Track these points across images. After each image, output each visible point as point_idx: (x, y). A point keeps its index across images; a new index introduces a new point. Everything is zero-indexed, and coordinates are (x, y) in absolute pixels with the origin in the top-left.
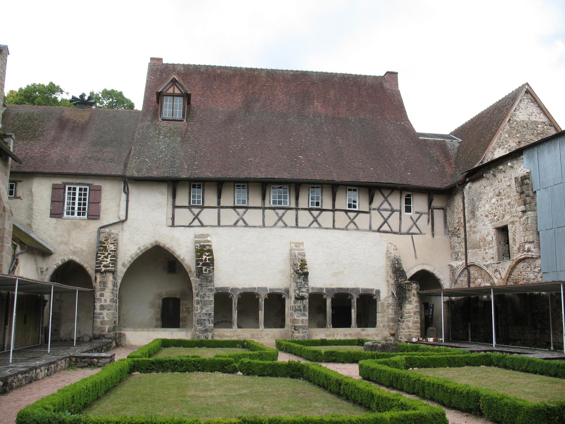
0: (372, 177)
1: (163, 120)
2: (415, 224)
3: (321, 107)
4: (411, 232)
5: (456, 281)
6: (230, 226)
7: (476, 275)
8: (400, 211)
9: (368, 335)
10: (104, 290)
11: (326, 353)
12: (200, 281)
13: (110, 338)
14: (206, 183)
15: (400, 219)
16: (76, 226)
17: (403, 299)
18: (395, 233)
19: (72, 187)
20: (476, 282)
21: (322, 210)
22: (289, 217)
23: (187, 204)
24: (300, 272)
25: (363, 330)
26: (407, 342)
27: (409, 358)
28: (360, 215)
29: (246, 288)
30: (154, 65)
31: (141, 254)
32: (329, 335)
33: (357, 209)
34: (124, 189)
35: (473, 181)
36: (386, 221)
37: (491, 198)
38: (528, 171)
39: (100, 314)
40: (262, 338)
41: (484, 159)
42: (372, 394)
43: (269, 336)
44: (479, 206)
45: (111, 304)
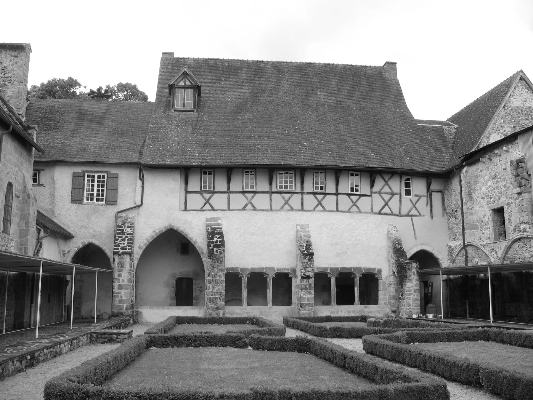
0: (373, 162)
1: (175, 111)
2: (414, 206)
3: (324, 96)
4: (410, 214)
5: (454, 260)
7: (473, 254)
9: (371, 312)
10: (122, 270)
12: (212, 262)
15: (400, 201)
18: (395, 215)
19: (91, 174)
20: (474, 261)
21: (326, 194)
22: (295, 200)
23: (199, 190)
25: (366, 307)
26: (407, 318)
27: (410, 333)
28: (362, 198)
31: (156, 237)
32: (334, 312)
33: (359, 193)
34: (140, 176)
35: (470, 165)
36: (386, 204)
37: (488, 181)
38: (523, 154)
39: (118, 293)
41: (480, 143)
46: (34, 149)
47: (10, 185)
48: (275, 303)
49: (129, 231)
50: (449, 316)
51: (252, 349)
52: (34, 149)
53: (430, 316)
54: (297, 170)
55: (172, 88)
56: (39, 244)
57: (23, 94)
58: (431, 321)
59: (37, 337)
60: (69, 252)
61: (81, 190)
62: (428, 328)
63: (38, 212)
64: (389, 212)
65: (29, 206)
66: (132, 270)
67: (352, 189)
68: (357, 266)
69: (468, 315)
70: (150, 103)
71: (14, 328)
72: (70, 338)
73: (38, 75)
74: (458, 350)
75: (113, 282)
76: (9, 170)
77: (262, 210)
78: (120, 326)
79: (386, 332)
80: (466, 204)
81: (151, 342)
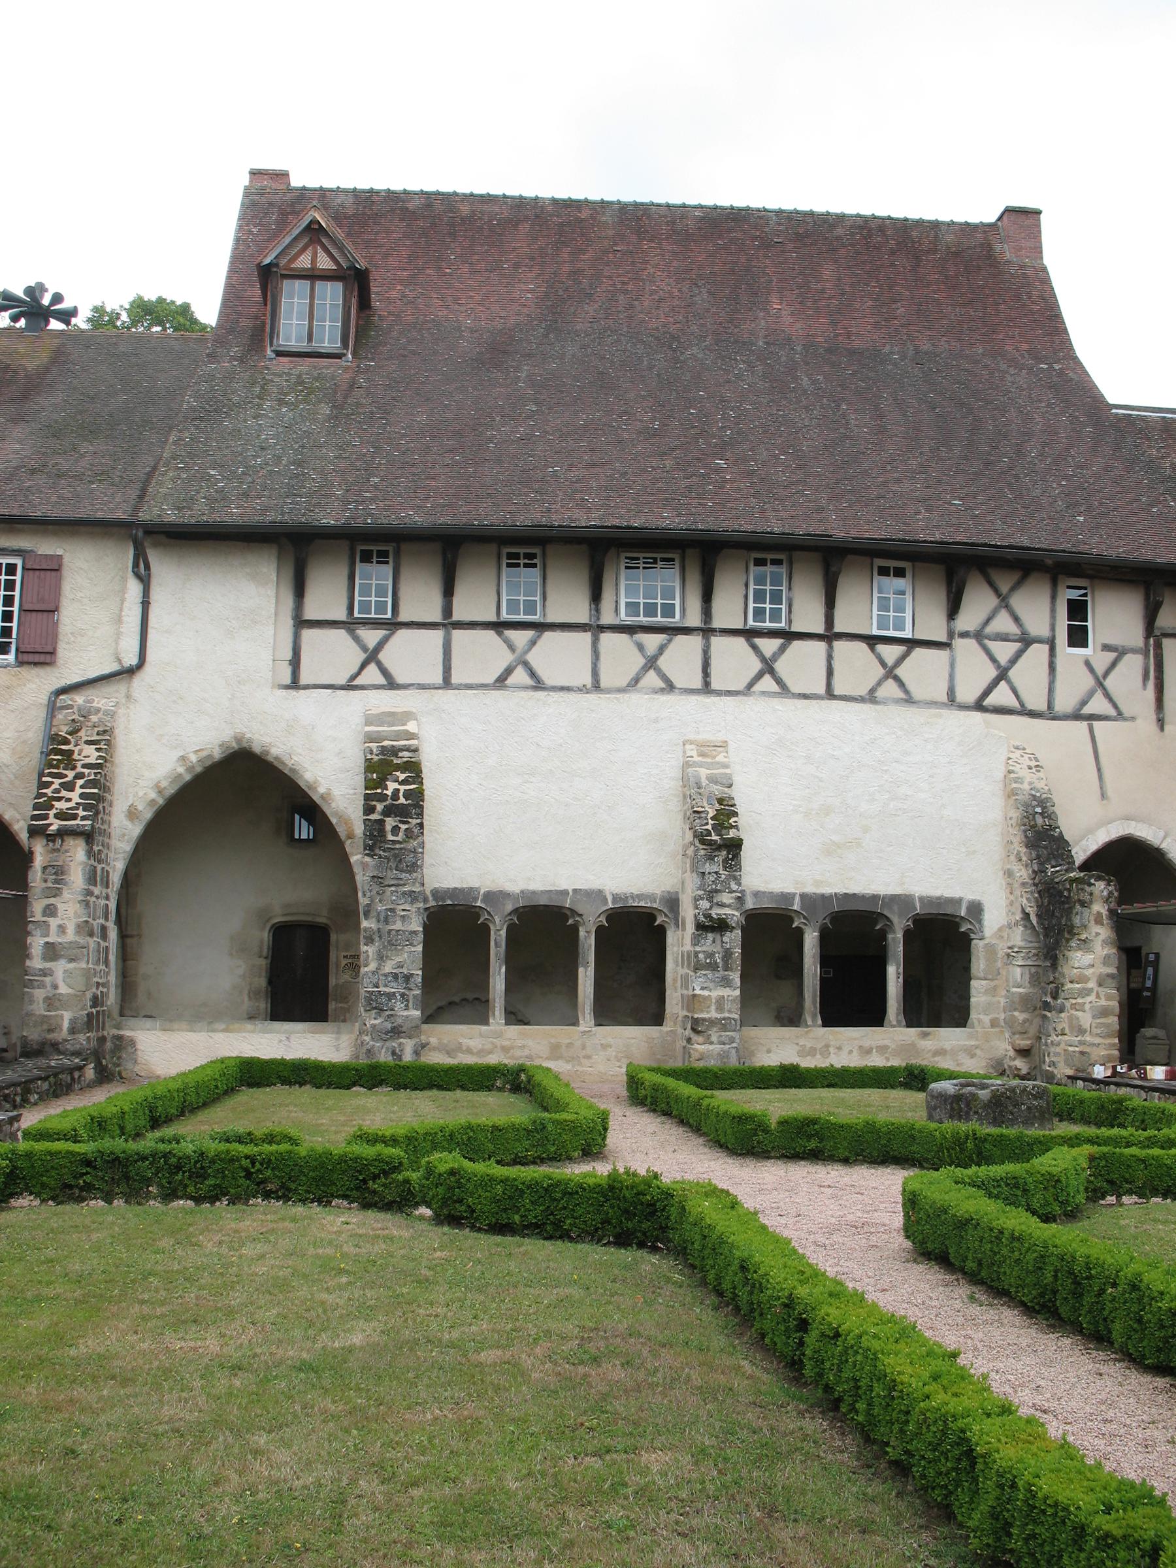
0: (959, 526)
1: (279, 354)
2: (1100, 684)
3: (792, 315)
4: (1087, 710)
9: (941, 1052)
10: (56, 893)
11: (783, 1123)
12: (378, 867)
13: (76, 1054)
14: (404, 547)
17: (1061, 932)
18: (1032, 714)
21: (790, 636)
22: (681, 657)
23: (341, 614)
24: (714, 837)
25: (926, 1035)
26: (1073, 1078)
27: (1104, 1156)
28: (919, 652)
29: (534, 892)
30: (262, 192)
31: (188, 777)
32: (812, 1052)
33: (907, 634)
34: (136, 565)
36: (1003, 675)
39: (45, 973)
40: (588, 1057)
42: (963, 1440)
43: (611, 1052)
45: (81, 940)
53: (1158, 1073)
54: (689, 551)
64: (1012, 702)
66: (97, 891)
77: (562, 689)
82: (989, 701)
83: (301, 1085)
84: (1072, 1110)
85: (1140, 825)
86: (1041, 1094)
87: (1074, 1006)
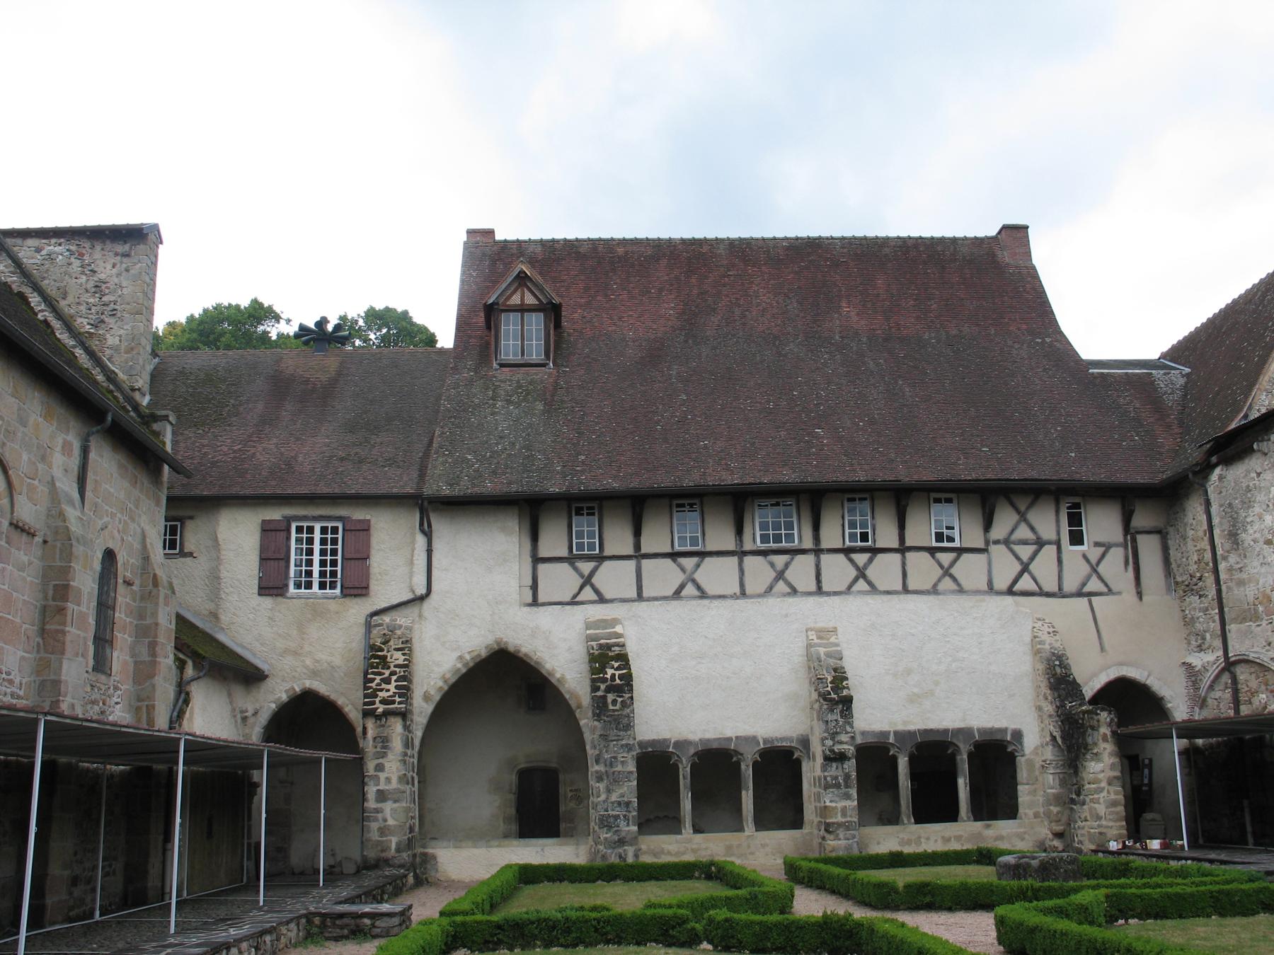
0: (988, 467)
1: (502, 365)
2: (1095, 570)
3: (858, 314)
4: (1087, 589)
5: (1204, 700)
6: (665, 598)
7: (1254, 684)
8: (1058, 544)
9: (1000, 838)
10: (384, 755)
12: (604, 728)
13: (401, 866)
15: (1060, 561)
16: (318, 613)
17: (1079, 749)
18: (1048, 595)
19: (305, 524)
20: (1256, 701)
21: (875, 551)
22: (801, 570)
23: (564, 552)
25: (988, 826)
26: (1095, 852)
27: (1114, 895)
28: (965, 556)
29: (708, 740)
31: (464, 670)
32: (909, 842)
33: (957, 544)
34: (421, 524)
35: (1228, 461)
36: (1025, 569)
39: (377, 811)
40: (752, 853)
41: (1250, 408)
44: (1249, 520)
45: (402, 788)
46: (166, 467)
47: (109, 555)
48: (761, 824)
49: (399, 658)
50: (1201, 841)
51: (710, 947)
52: (166, 467)
53: (1155, 845)
55: (492, 312)
56: (183, 696)
57: (144, 341)
58: (1158, 857)
59: (172, 931)
60: (255, 714)
61: (282, 563)
62: (1159, 879)
63: (180, 619)
65: (157, 604)
66: (409, 752)
67: (939, 537)
68: (962, 725)
69: (1250, 839)
70: (443, 351)
71: (125, 904)
72: (254, 930)
73: (178, 298)
74: (1252, 939)
75: (364, 784)
76: (106, 519)
78: (383, 892)
79: (1051, 893)
80: (1225, 558)
81: (455, 937)
82: (1017, 587)
83: (561, 881)
84: (1095, 872)
85: (1130, 669)
86: (1073, 861)
87: (1092, 800)
